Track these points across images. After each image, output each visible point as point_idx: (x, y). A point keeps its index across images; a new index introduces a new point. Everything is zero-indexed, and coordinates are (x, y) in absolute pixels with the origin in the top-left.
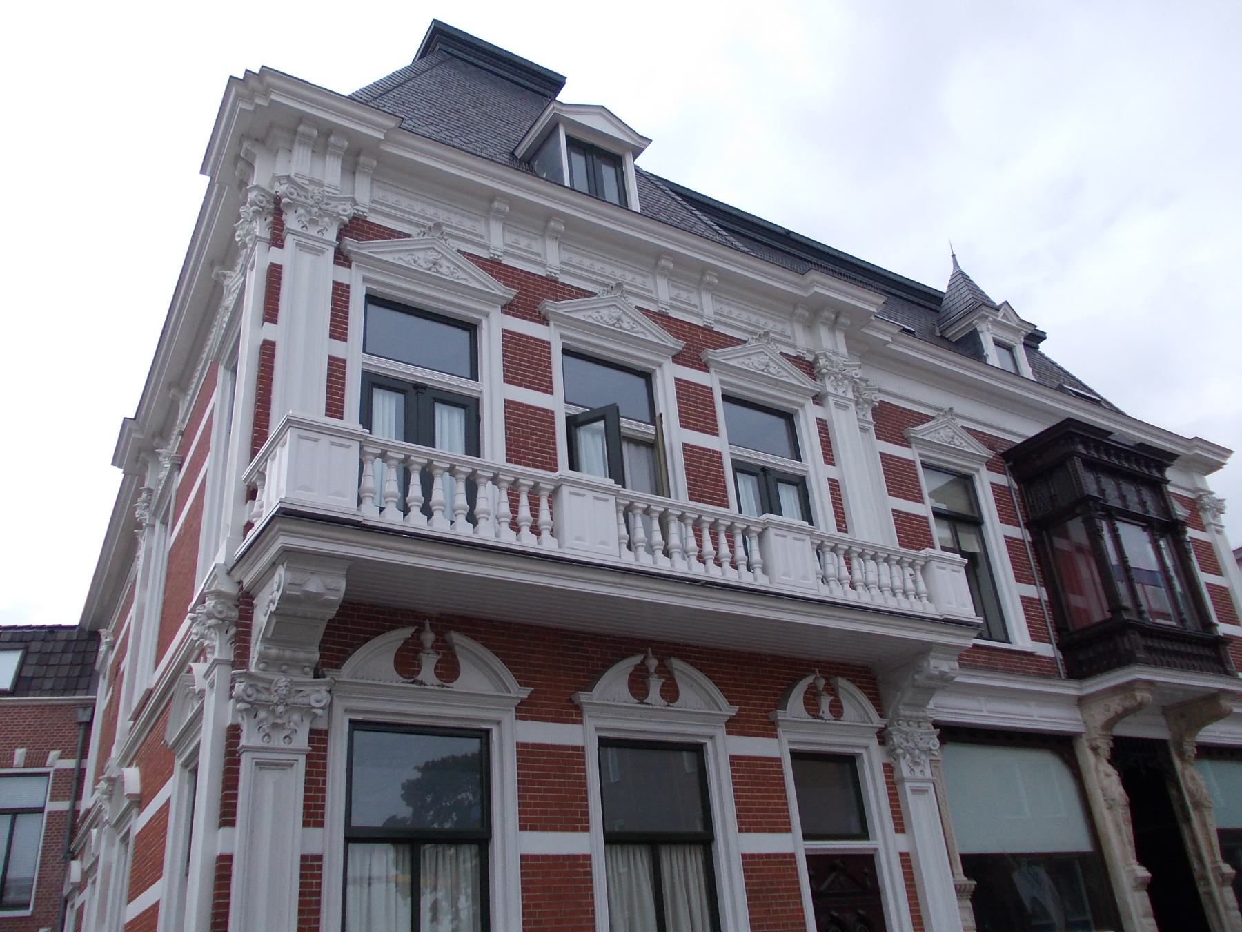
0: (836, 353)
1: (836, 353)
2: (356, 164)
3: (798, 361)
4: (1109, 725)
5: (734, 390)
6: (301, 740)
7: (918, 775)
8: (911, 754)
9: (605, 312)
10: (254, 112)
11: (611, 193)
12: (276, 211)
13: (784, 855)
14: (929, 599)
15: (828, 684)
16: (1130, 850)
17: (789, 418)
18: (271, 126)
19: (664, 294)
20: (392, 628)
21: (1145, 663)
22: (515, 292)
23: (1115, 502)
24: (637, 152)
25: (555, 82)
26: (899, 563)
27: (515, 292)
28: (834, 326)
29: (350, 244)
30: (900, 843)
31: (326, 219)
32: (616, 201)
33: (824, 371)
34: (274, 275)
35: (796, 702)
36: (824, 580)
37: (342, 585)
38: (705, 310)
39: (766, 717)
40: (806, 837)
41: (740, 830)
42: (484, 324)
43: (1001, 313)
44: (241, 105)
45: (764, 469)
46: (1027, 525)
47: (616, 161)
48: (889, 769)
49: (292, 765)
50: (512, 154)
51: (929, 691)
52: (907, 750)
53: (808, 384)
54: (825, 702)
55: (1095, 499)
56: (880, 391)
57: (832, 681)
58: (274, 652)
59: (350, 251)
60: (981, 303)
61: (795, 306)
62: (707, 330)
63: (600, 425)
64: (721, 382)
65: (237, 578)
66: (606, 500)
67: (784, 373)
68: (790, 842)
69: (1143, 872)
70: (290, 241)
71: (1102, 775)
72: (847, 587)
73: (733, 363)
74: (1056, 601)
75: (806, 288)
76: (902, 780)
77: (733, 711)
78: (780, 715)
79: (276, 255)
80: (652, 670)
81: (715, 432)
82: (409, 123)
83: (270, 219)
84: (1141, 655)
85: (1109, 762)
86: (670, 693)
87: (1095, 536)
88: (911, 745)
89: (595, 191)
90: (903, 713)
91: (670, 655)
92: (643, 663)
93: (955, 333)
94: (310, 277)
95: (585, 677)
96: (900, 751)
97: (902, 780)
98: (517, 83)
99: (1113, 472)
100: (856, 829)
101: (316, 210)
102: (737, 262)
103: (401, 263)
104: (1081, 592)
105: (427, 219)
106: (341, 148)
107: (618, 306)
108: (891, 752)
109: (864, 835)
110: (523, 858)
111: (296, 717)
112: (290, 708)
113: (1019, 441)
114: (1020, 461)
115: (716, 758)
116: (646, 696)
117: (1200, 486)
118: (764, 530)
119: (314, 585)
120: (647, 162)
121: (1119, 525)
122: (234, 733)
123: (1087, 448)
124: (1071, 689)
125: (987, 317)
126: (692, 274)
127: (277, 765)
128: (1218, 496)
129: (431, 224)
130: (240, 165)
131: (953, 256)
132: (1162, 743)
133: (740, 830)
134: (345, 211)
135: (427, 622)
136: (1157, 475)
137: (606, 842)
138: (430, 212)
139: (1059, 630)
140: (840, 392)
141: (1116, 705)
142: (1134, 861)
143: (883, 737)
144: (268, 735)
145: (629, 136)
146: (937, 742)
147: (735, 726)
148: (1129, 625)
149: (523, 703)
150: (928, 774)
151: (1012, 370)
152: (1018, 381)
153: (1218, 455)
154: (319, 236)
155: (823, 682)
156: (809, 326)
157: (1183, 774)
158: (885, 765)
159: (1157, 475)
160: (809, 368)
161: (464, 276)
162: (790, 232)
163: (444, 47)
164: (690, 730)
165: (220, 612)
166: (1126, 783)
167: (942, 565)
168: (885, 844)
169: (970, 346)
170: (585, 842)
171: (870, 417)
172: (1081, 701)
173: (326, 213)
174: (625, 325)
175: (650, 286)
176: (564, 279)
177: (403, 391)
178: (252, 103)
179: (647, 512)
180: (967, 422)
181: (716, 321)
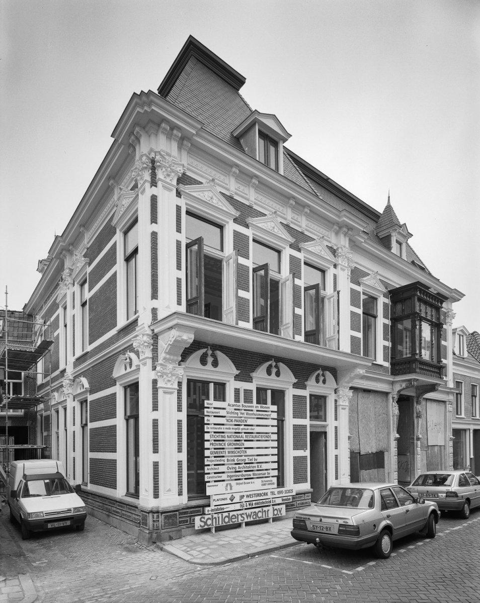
0: (344, 247)
1: (344, 247)
2: (182, 144)
3: (330, 248)
4: (399, 392)
5: (309, 261)
6: (176, 386)
10: (144, 113)
13: (304, 425)
15: (276, 365)
16: (395, 429)
20: (268, 361)
23: (423, 315)
24: (285, 140)
28: (170, 136)
29: (182, 187)
30: (335, 423)
31: (173, 174)
32: (274, 169)
38: (303, 224)
42: (227, 226)
43: (402, 229)
44: (138, 109)
47: (276, 144)
48: (336, 401)
55: (418, 313)
57: (278, 364)
59: (181, 190)
62: (250, 207)
64: (186, 204)
65: (152, 328)
68: (306, 422)
69: (398, 436)
70: (160, 184)
73: (260, 225)
74: (394, 348)
75: (339, 217)
77: (238, 372)
79: (154, 191)
83: (150, 171)
84: (418, 370)
85: (397, 402)
87: (414, 326)
91: (280, 362)
92: (206, 352)
94: (168, 202)
99: (426, 303)
101: (169, 169)
112: (173, 375)
113: (398, 286)
114: (397, 296)
117: (449, 307)
122: (155, 382)
123: (420, 293)
124: (391, 379)
125: (396, 230)
131: (389, 197)
134: (180, 170)
135: (209, 347)
136: (440, 305)
140: (343, 264)
142: (396, 432)
143: (336, 391)
148: (416, 360)
149: (237, 375)
151: (399, 255)
152: (400, 260)
153: (459, 296)
156: (337, 233)
159: (440, 305)
160: (334, 252)
169: (385, 242)
171: (350, 274)
172: (393, 383)
173: (173, 171)
174: (214, 201)
175: (227, 181)
178: (143, 109)
180: (381, 278)
181: (236, 193)
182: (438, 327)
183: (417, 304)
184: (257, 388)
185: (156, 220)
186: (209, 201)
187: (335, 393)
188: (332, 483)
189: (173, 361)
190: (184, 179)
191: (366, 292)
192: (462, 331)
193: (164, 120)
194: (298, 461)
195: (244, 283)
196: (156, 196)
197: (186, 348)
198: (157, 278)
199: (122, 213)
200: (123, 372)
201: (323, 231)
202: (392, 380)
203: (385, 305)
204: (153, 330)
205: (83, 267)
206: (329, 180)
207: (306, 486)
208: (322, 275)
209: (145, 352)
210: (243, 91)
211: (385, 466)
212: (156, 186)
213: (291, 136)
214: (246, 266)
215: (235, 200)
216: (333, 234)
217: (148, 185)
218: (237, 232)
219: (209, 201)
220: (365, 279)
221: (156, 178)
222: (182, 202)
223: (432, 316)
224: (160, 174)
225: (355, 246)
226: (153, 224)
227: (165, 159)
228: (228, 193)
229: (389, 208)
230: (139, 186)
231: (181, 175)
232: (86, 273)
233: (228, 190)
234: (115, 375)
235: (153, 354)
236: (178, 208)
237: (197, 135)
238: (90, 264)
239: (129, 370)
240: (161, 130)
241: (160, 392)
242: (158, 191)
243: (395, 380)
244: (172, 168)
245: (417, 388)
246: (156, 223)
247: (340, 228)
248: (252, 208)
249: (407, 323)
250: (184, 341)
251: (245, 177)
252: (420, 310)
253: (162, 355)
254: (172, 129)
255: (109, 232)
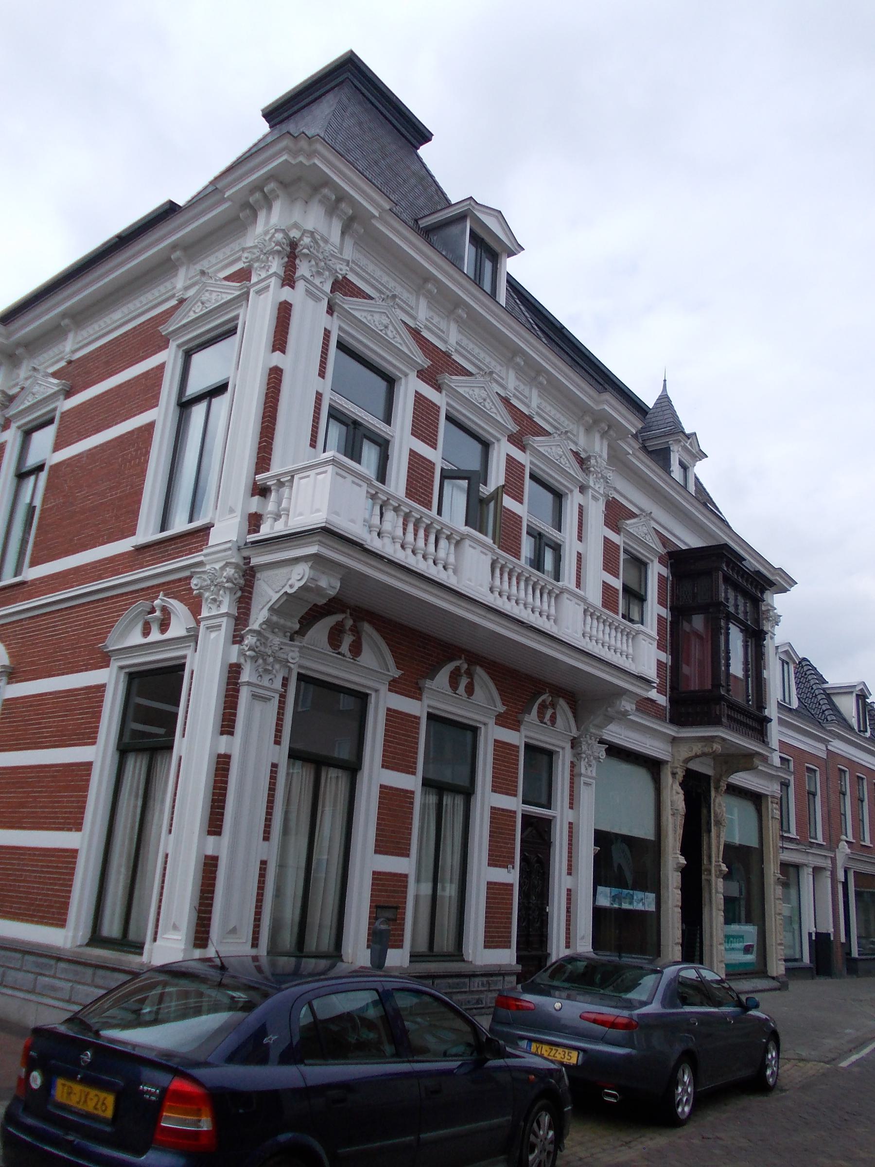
0: (600, 456)
3: (576, 454)
4: (687, 760)
6: (278, 684)
7: (589, 773)
8: (265, 660)
9: (377, 317)
11: (487, 287)
12: (292, 253)
14: (555, 621)
17: (391, 381)
18: (300, 179)
19: (422, 313)
21: (729, 727)
22: (429, 363)
23: (732, 609)
24: (511, 254)
25: (424, 136)
26: (598, 618)
27: (429, 363)
28: (604, 435)
29: (339, 297)
31: (327, 273)
33: (592, 469)
34: (284, 312)
35: (443, 678)
36: (491, 590)
37: (338, 585)
39: (516, 717)
40: (524, 803)
41: (383, 766)
45: (540, 534)
46: (672, 609)
48: (573, 765)
49: (270, 699)
50: (416, 221)
51: (610, 719)
52: (588, 756)
53: (580, 476)
54: (464, 682)
56: (615, 489)
58: (275, 618)
59: (336, 303)
60: (676, 429)
61: (585, 413)
62: (447, 355)
63: (465, 483)
64: (340, 328)
65: (246, 553)
66: (360, 486)
67: (494, 410)
68: (513, 804)
69: (683, 861)
70: (301, 285)
71: (674, 792)
72: (398, 546)
74: (675, 668)
76: (580, 775)
78: (428, 684)
79: (286, 294)
80: (347, 628)
81: (434, 446)
82: (397, 209)
83: (286, 259)
84: (724, 720)
85: (680, 784)
86: (356, 649)
88: (590, 752)
89: (478, 281)
90: (591, 730)
93: (653, 444)
94: (311, 321)
95: (427, 668)
96: (584, 756)
97: (580, 775)
98: (382, 113)
99: (736, 587)
100: (544, 800)
101: (323, 264)
102: (530, 344)
103: (364, 320)
104: (688, 664)
105: (387, 289)
106: (345, 214)
107: (486, 389)
108: (577, 755)
109: (548, 806)
110: (382, 786)
111: (277, 666)
113: (684, 547)
114: (680, 561)
115: (376, 707)
116: (339, 647)
118: (462, 539)
119: (323, 583)
120: (512, 266)
121: (731, 625)
122: (234, 672)
123: (727, 566)
125: (680, 441)
126: (532, 373)
127: (262, 697)
128: (778, 611)
129: (388, 293)
130: (258, 195)
131: (665, 381)
132: (708, 777)
133: (383, 766)
135: (348, 611)
137: (423, 785)
138: (392, 284)
139: (672, 688)
141: (697, 749)
142: (679, 852)
143: (575, 743)
144: (261, 676)
145: (512, 244)
146: (604, 753)
147: (395, 686)
150: (594, 775)
154: (320, 285)
155: (465, 666)
156: (588, 430)
157: (714, 801)
158: (572, 762)
160: (582, 462)
161: (400, 341)
162: (564, 327)
163: (351, 77)
164: (460, 712)
165: (236, 579)
166: (687, 800)
167: (571, 598)
168: (560, 814)
169: (661, 457)
170: (411, 782)
172: (674, 740)
173: (328, 268)
174: (389, 333)
175: (412, 302)
176: (456, 357)
177: (347, 425)
179: (527, 580)
182: (756, 636)
183: (722, 587)
184: (429, 714)
185: (285, 347)
186: (381, 331)
187: (572, 747)
188: (557, 950)
189: (283, 629)
190: (342, 286)
191: (630, 549)
192: (786, 652)
193: (327, 182)
194: (496, 891)
195: (423, 493)
196: (291, 305)
197: (315, 605)
198: (271, 454)
199: (192, 316)
200: (136, 638)
201: (567, 423)
202: (673, 734)
203: (661, 578)
204: (247, 559)
205: (53, 396)
206: (564, 330)
207: (506, 957)
208: (554, 501)
209: (221, 602)
210: (424, 151)
211: (722, 902)
212: (293, 287)
213: (523, 249)
214: (430, 462)
215: (423, 337)
216: (582, 431)
217: (274, 282)
218: (421, 395)
219: (381, 331)
220: (628, 522)
221: (295, 273)
222: (334, 325)
223: (746, 613)
224: (303, 269)
225: (616, 459)
226: (278, 352)
227: (319, 246)
228: (411, 323)
229: (664, 400)
230: (254, 279)
231: (340, 277)
232: (55, 409)
233: (414, 318)
234: (113, 643)
235: (239, 608)
236: (327, 334)
237: (381, 218)
238: (69, 393)
239: (155, 636)
240: (318, 197)
241: (244, 694)
242: (296, 296)
243: (680, 735)
244: (328, 262)
245: (715, 757)
246: (284, 352)
247: (596, 422)
248: (450, 358)
249: (698, 622)
250: (319, 590)
251: (449, 305)
252: (727, 599)
253: (259, 617)
254: (339, 200)
255: (148, 339)
